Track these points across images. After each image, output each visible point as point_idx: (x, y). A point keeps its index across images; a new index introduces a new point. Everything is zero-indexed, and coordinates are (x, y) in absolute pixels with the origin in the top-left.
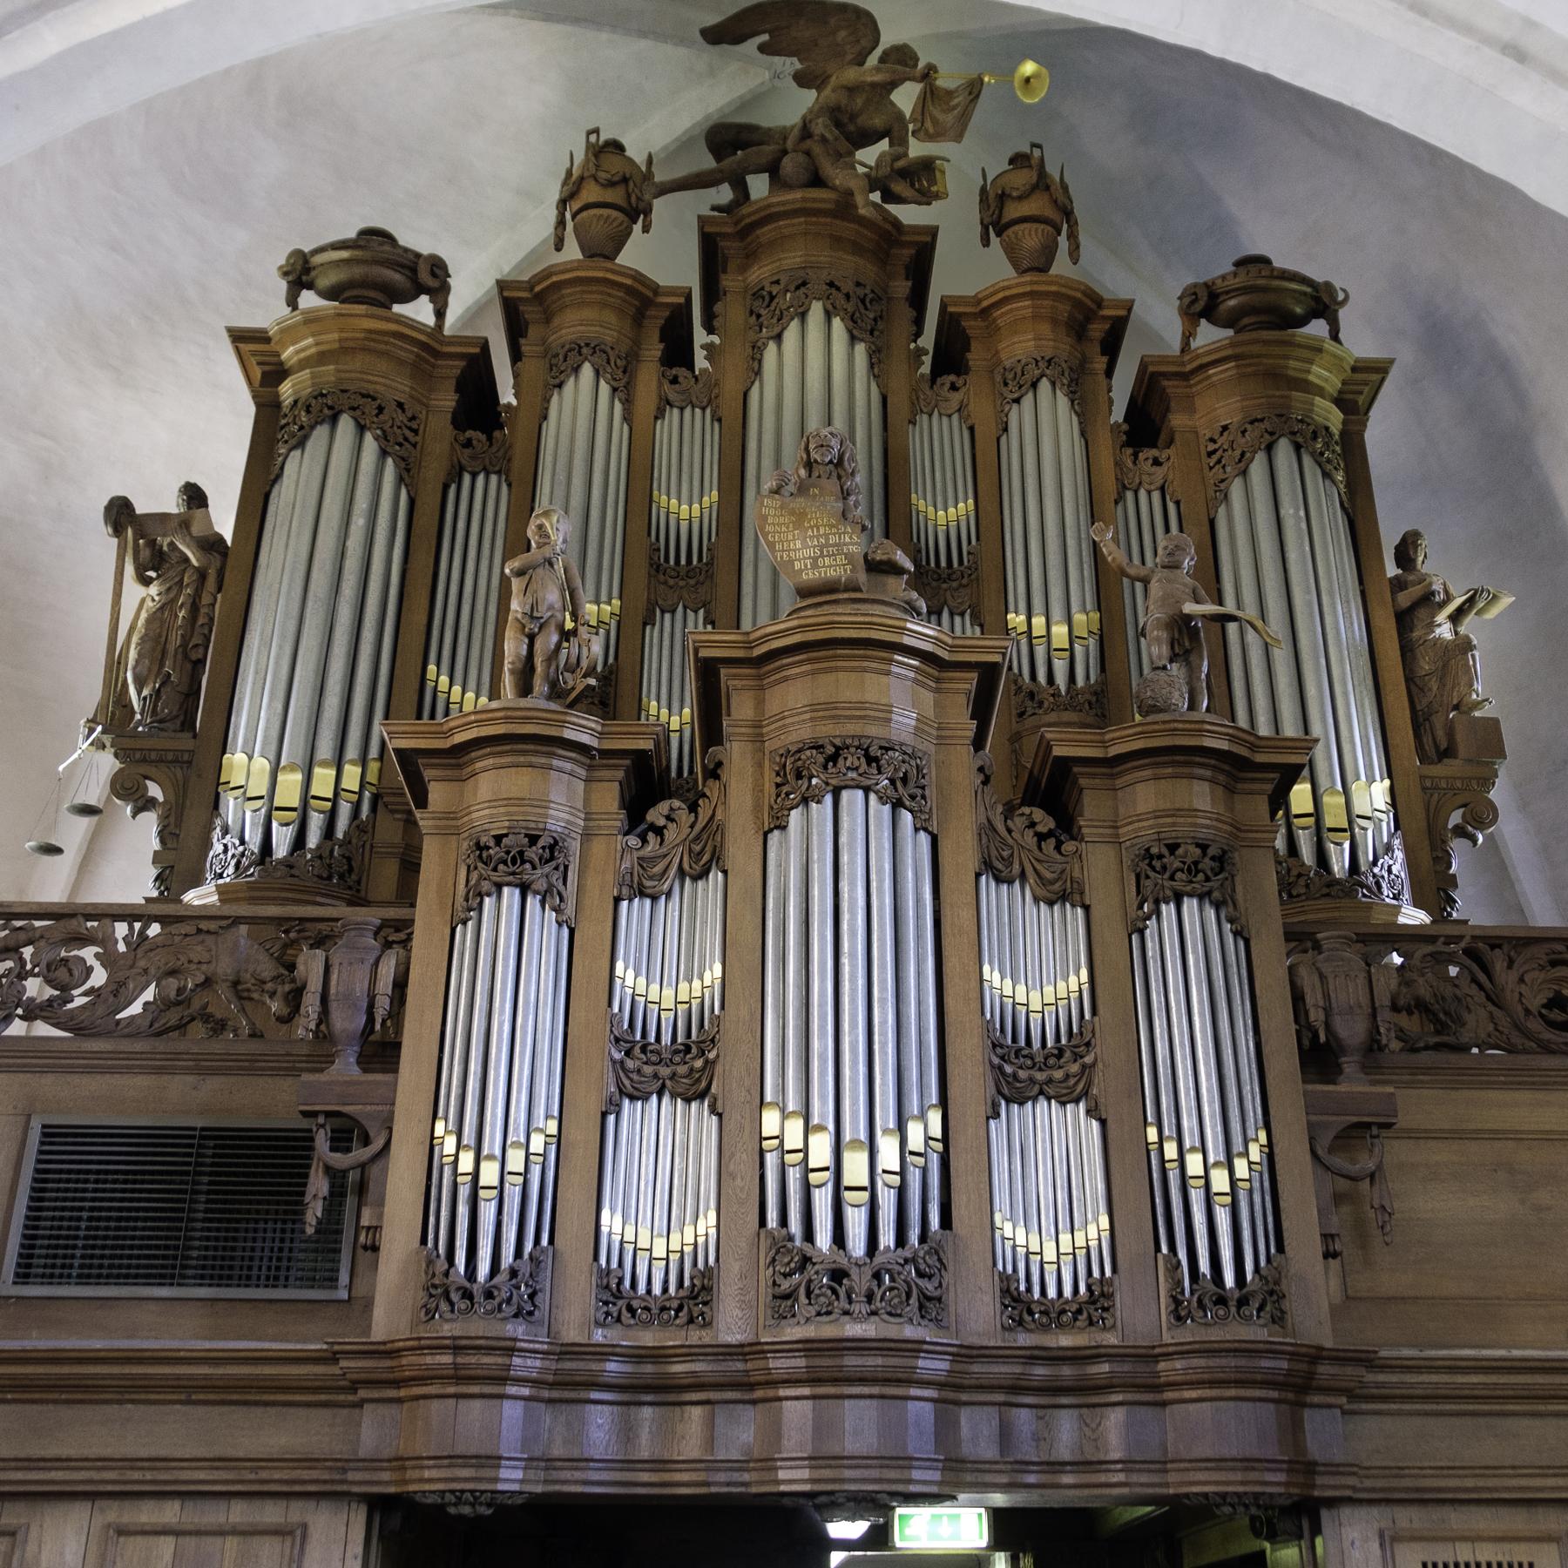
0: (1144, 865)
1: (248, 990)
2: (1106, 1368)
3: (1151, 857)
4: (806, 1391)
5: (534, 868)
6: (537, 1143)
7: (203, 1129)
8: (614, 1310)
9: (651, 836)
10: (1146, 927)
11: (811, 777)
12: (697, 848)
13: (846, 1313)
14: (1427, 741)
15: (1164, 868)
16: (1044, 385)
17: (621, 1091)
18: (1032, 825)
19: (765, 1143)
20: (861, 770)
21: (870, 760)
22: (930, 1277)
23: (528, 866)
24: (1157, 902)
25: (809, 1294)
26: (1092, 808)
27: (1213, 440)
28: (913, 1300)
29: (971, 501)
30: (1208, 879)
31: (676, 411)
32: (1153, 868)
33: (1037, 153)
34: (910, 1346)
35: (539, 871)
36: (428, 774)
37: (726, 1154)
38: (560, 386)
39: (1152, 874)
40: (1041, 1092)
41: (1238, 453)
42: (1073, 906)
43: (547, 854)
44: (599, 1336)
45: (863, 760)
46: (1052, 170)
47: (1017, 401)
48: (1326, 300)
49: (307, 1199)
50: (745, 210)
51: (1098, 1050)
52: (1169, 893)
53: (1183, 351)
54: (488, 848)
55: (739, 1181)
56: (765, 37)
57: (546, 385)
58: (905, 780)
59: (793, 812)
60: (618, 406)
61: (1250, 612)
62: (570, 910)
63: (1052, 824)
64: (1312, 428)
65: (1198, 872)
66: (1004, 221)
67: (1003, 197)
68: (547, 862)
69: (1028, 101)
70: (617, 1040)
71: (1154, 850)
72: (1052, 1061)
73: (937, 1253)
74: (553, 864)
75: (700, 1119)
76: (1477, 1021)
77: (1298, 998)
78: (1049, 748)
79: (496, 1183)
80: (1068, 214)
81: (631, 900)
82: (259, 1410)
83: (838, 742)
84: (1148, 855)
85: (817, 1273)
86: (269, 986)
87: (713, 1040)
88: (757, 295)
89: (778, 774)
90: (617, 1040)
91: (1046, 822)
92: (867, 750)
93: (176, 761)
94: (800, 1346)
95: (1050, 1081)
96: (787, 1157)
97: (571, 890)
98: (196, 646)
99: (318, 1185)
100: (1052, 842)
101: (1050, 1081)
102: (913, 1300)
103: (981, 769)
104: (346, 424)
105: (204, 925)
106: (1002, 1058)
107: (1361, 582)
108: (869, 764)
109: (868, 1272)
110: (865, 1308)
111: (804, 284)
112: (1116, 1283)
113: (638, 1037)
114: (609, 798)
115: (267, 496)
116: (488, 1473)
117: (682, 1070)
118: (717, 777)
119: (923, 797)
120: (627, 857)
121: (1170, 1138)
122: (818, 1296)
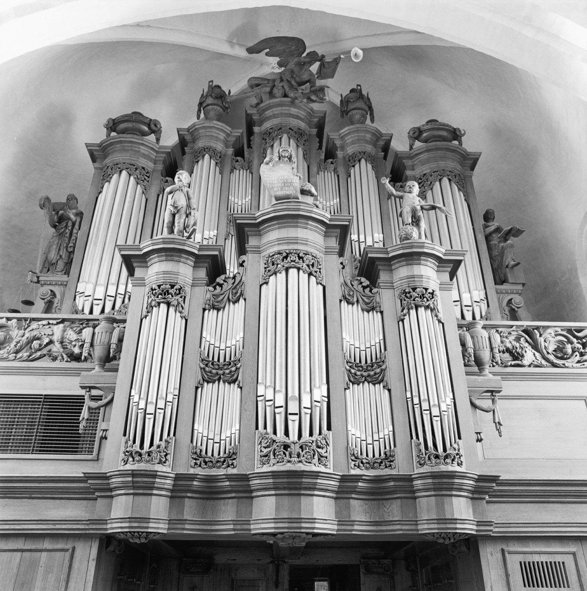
0: (403, 296)
1: (66, 345)
2: (392, 483)
3: (406, 293)
4: (273, 492)
5: (172, 296)
6: (170, 398)
7: (45, 395)
8: (198, 462)
9: (218, 287)
10: (404, 319)
11: (278, 264)
12: (234, 291)
13: (289, 462)
14: (497, 277)
15: (411, 296)
16: (363, 161)
17: (203, 380)
18: (361, 283)
19: (259, 399)
20: (296, 261)
21: (300, 258)
22: (323, 448)
23: (170, 296)
24: (409, 310)
25: (274, 454)
26: (383, 277)
27: (421, 179)
28: (316, 457)
29: (338, 199)
30: (428, 300)
31: (238, 171)
32: (407, 297)
33: (359, 88)
34: (314, 474)
35: (174, 298)
36: (135, 264)
37: (243, 401)
38: (198, 162)
39: (406, 299)
40: (365, 380)
41: (429, 182)
42: (377, 312)
43: (178, 292)
44: (192, 471)
45: (297, 258)
46: (364, 93)
47: (354, 166)
48: (458, 134)
49: (81, 418)
50: (262, 105)
51: (387, 363)
52: (413, 305)
53: (410, 150)
54: (155, 289)
55: (248, 413)
56: (268, 50)
57: (193, 163)
58: (313, 265)
59: (271, 277)
60: (218, 169)
61: (441, 205)
62: (185, 312)
63: (368, 283)
64: (454, 174)
65: (424, 298)
66: (348, 109)
67: (348, 102)
68: (177, 294)
69: (354, 60)
70: (203, 360)
71: (407, 291)
72: (369, 368)
73: (325, 439)
74: (180, 295)
75: (233, 389)
76: (530, 356)
77: (463, 345)
78: (367, 254)
79: (153, 412)
80: (370, 108)
81: (209, 310)
82: (58, 501)
83: (287, 251)
84: (405, 292)
85: (278, 446)
86: (74, 343)
87: (239, 360)
88: (265, 133)
89: (265, 264)
90: (203, 360)
91: (366, 282)
92: (298, 255)
93: (62, 285)
94: (270, 474)
95: (369, 376)
96: (267, 403)
97: (186, 306)
98: (71, 247)
99: (85, 414)
100: (369, 289)
101: (369, 376)
102: (316, 457)
103: (342, 263)
104: (124, 173)
105: (51, 322)
106: (350, 367)
107: (473, 225)
108: (299, 259)
109: (298, 446)
110: (296, 459)
111: (281, 129)
112: (395, 451)
113: (211, 359)
114: (202, 273)
115: (97, 198)
116: (145, 525)
117: (227, 371)
118: (243, 266)
119: (320, 272)
120: (208, 293)
121: (416, 396)
122: (278, 455)
